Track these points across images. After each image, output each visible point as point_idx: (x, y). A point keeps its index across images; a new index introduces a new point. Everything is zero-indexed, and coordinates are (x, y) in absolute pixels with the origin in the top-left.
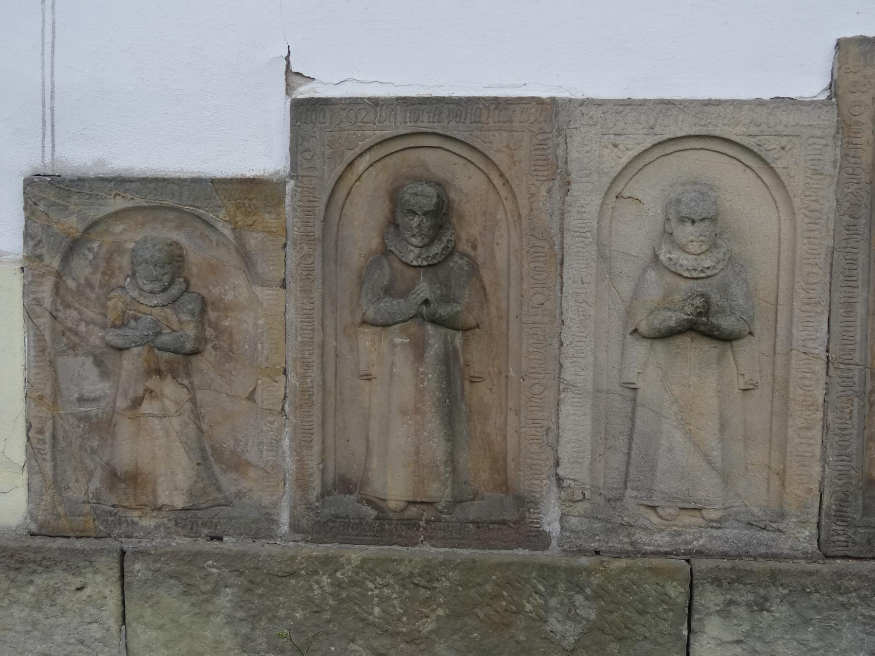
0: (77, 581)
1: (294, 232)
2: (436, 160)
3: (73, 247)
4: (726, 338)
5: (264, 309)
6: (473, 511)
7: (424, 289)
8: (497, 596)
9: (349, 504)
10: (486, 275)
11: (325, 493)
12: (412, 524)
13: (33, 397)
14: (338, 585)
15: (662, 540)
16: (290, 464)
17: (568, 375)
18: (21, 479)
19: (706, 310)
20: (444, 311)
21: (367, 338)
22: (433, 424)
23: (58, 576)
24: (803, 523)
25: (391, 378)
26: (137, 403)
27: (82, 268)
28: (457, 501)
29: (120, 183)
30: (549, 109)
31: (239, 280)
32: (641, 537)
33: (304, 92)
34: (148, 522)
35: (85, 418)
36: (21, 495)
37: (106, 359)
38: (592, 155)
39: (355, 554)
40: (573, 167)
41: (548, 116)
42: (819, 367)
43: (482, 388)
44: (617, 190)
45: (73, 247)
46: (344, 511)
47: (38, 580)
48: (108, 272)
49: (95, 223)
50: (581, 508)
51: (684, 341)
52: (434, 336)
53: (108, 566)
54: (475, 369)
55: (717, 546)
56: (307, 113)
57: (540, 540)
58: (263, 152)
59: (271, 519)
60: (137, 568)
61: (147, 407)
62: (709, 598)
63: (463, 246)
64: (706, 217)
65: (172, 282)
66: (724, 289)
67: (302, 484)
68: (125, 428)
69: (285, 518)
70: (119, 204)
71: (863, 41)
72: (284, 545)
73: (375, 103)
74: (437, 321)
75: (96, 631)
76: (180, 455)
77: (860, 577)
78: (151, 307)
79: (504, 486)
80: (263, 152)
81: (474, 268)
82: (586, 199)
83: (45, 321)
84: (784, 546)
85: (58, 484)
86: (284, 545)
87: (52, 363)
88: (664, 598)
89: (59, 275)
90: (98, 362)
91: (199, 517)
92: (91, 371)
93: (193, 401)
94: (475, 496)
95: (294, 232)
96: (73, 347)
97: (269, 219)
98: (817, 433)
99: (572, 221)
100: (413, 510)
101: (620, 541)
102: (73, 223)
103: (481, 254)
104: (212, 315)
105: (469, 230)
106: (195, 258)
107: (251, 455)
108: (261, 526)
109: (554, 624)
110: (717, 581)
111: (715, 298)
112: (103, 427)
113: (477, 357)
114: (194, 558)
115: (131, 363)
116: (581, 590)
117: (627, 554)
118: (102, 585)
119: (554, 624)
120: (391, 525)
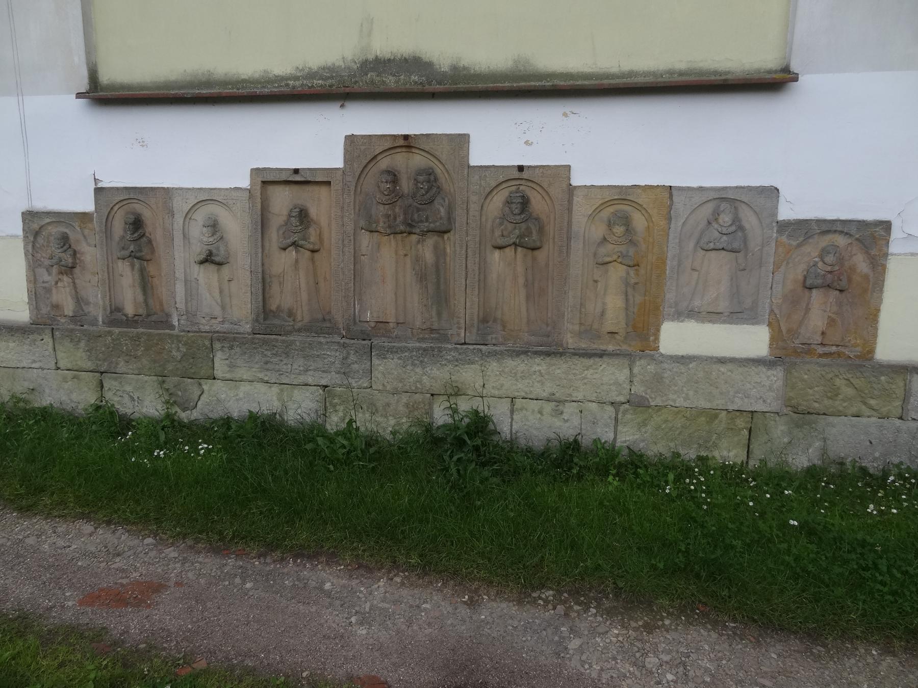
0: (41, 338)
1: (97, 229)
2: (139, 208)
3: (37, 234)
4: (220, 264)
5: (91, 253)
6: (154, 318)
7: (132, 248)
8: (157, 344)
9: (118, 315)
10: (154, 243)
11: (111, 312)
12: (136, 322)
13: (29, 281)
14: (113, 339)
15: (207, 328)
16: (101, 303)
17: (177, 275)
18: (27, 307)
19: (210, 254)
20: (138, 255)
21: (120, 263)
22: (139, 291)
23: (36, 336)
24: (663, 401)
25: (127, 276)
26: (57, 283)
27: (40, 240)
28: (148, 315)
29: (49, 214)
30: (167, 191)
31: (84, 244)
32: (201, 327)
33: (100, 185)
34: (63, 320)
35: (45, 288)
36: (28, 311)
37: (48, 269)
38: (181, 206)
39: (117, 330)
40: (175, 209)
41: (167, 192)
42: (248, 273)
43: (155, 280)
44: (189, 216)
45: (37, 234)
46: (116, 316)
47: (30, 337)
48: (49, 242)
49: (42, 227)
50: (184, 317)
51: (207, 264)
52: (137, 263)
53: (48, 332)
54: (152, 273)
55: (221, 330)
56: (99, 191)
57: (172, 327)
58: (86, 204)
59: (96, 320)
60: (57, 333)
61: (60, 284)
62: (217, 345)
63: (147, 234)
64: (214, 226)
65: (64, 245)
66: (218, 249)
67: (105, 310)
68: (54, 291)
69: (100, 320)
70: (48, 220)
71: (258, 169)
72: (101, 328)
73: (117, 189)
74: (138, 258)
75: (47, 353)
76: (69, 298)
77: (259, 339)
78: (58, 253)
79: (163, 310)
80: (86, 204)
81: (150, 242)
82: (179, 219)
83: (30, 257)
84: (242, 330)
85: (37, 308)
86: (101, 328)
87: (34, 271)
88: (204, 345)
89: (33, 242)
90: (47, 270)
91: (78, 318)
92: (46, 273)
93: (74, 283)
94: (155, 313)
95: (97, 229)
96: (40, 265)
97: (90, 225)
98: (249, 294)
99: (175, 225)
100: (136, 318)
101: (195, 328)
102: (36, 226)
103: (152, 237)
104: (78, 255)
105: (149, 229)
106: (72, 236)
107: (91, 300)
108: (94, 322)
109: (174, 353)
110: (219, 340)
111: (214, 251)
112: (48, 291)
113: (151, 269)
114: (72, 330)
115: (55, 270)
116: (180, 342)
117: (197, 332)
118: (48, 339)
119: (174, 353)
120: (131, 322)
